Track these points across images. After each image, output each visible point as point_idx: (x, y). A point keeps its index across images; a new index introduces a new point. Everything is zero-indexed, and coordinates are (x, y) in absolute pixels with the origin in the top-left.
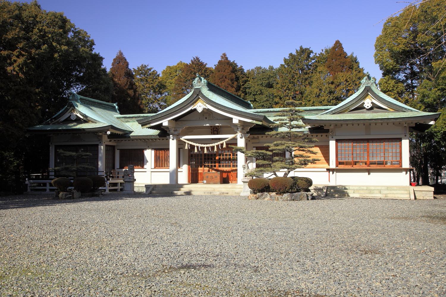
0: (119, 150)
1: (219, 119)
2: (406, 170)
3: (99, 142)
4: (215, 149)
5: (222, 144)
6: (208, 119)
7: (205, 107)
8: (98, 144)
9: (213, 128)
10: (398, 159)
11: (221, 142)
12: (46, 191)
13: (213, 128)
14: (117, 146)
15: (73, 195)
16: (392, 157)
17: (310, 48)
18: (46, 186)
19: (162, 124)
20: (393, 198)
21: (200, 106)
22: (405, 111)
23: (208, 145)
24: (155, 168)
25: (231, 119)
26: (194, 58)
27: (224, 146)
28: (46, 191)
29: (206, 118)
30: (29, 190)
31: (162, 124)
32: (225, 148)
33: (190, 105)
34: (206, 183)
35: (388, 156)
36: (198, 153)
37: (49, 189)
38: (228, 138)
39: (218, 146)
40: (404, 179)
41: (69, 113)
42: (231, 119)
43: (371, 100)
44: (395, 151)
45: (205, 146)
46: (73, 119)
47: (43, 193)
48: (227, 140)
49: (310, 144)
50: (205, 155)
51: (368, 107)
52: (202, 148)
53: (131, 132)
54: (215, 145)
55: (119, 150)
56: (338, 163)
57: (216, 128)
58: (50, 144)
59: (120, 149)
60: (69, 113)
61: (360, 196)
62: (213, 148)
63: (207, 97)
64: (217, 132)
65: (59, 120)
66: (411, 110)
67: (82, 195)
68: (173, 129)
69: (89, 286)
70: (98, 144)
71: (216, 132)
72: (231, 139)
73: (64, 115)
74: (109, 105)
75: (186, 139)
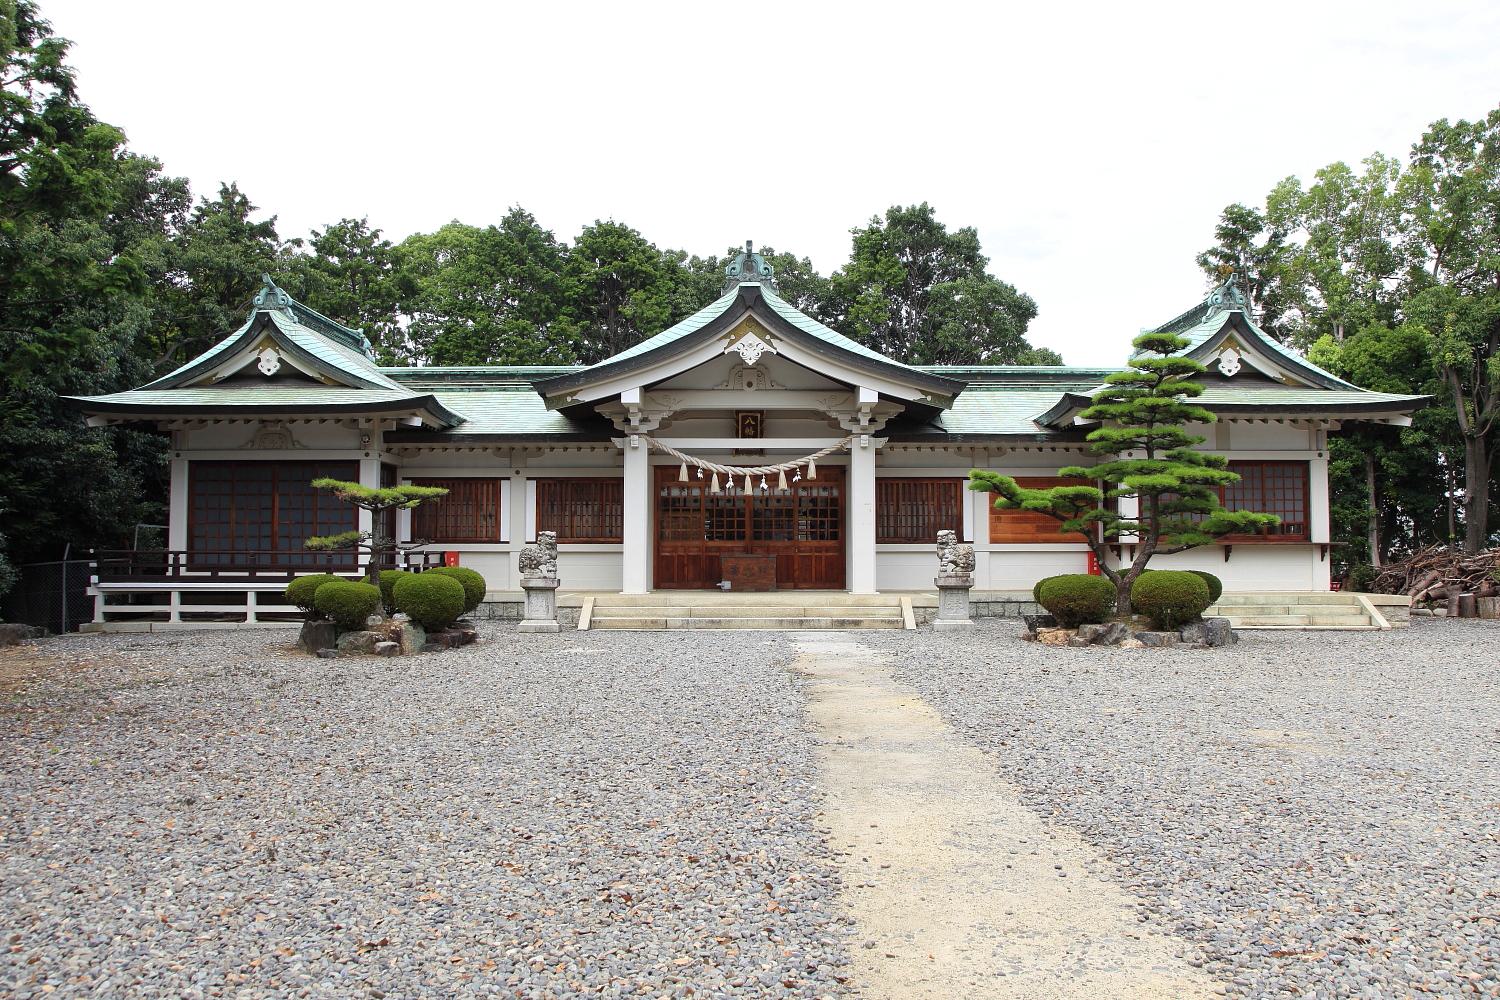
1: (793, 390)
2: (1323, 548)
3: (364, 452)
4: (783, 484)
5: (804, 468)
7: (768, 348)
8: (358, 461)
9: (743, 417)
10: (1300, 518)
11: (801, 461)
13: (744, 418)
14: (402, 467)
19: (618, 396)
20: (1337, 627)
21: (751, 348)
23: (756, 471)
24: (412, 542)
25: (852, 389)
27: (812, 473)
29: (750, 385)
30: (98, 618)
31: (618, 396)
32: (812, 481)
33: (720, 339)
34: (729, 591)
35: (1294, 511)
36: (722, 494)
38: (821, 449)
39: (790, 474)
40: (1319, 572)
42: (852, 389)
43: (1239, 354)
45: (747, 471)
46: (269, 374)
47: (158, 625)
48: (820, 454)
50: (715, 499)
51: (1230, 371)
52: (739, 480)
53: (462, 421)
54: (782, 467)
57: (751, 417)
61: (1242, 624)
62: (773, 479)
63: (293, 339)
64: (755, 429)
65: (216, 374)
67: (427, 641)
68: (640, 416)
70: (358, 461)
72: (832, 453)
74: (348, 335)
75: (681, 450)
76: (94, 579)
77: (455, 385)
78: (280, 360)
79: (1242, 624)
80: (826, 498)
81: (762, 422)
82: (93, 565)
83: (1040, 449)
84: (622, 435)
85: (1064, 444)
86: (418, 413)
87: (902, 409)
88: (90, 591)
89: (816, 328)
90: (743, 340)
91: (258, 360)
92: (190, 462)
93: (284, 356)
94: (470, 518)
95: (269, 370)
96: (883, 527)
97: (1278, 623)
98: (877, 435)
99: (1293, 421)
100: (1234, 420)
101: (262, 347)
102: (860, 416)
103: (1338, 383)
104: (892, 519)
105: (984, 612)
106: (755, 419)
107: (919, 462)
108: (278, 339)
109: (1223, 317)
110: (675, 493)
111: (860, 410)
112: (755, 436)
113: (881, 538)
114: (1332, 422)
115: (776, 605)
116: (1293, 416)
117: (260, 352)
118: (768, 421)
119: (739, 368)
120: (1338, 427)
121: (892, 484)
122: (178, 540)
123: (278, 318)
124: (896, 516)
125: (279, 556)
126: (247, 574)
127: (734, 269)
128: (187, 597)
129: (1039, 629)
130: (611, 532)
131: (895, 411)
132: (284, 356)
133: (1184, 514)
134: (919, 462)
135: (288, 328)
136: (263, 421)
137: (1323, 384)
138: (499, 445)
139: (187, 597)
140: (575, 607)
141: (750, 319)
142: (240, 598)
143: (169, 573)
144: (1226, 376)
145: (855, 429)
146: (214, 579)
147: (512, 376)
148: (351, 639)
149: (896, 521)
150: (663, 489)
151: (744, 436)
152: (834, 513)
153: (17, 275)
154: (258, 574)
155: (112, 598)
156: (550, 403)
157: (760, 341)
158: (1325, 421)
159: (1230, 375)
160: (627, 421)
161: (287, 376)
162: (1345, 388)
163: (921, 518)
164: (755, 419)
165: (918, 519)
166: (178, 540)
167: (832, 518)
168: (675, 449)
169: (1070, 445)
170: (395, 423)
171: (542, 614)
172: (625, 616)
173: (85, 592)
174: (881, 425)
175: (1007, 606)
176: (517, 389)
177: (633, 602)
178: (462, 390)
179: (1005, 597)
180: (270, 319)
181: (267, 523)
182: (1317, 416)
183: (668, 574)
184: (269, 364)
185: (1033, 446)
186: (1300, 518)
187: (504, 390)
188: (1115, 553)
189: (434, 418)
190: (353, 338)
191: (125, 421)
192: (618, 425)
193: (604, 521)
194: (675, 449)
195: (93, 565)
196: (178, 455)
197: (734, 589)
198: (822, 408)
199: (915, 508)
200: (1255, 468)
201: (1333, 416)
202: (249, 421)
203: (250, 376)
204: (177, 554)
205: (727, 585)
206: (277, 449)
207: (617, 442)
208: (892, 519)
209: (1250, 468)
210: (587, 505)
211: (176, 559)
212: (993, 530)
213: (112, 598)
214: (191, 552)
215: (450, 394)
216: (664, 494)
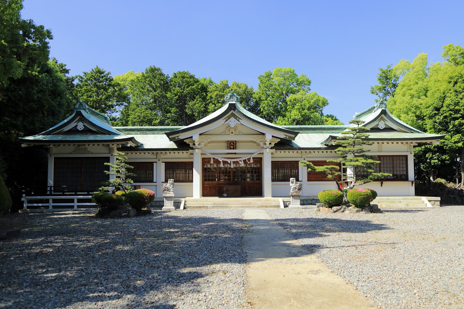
0: (164, 163)
5: (249, 159)
6: (234, 134)
9: (230, 143)
12: (49, 209)
13: (230, 143)
15: (129, 213)
16: (384, 167)
17: (83, 72)
18: (48, 202)
22: (413, 132)
26: (108, 74)
28: (49, 208)
29: (232, 133)
37: (52, 206)
41: (75, 122)
44: (404, 165)
49: (330, 159)
55: (164, 163)
56: (204, 169)
58: (48, 156)
59: (165, 162)
60: (75, 122)
64: (234, 146)
65: (63, 130)
66: (422, 133)
69: (35, 301)
71: (232, 147)
73: (69, 125)
76: (24, 195)
77: (138, 132)
78: (84, 126)
79: (386, 206)
80: (256, 168)
81: (236, 144)
82: (24, 191)
83: (323, 152)
84: (192, 149)
85: (330, 151)
86: (129, 142)
87: (279, 140)
88: (23, 199)
89: (252, 116)
90: (230, 120)
91: (77, 126)
92: (55, 158)
93: (85, 124)
94: (184, 174)
95: (80, 129)
96: (274, 177)
97: (397, 206)
98: (272, 148)
99: (402, 143)
100: (383, 143)
101: (78, 121)
102: (266, 143)
103: (416, 131)
104: (277, 174)
105: (306, 203)
106: (234, 143)
107: (285, 155)
108: (83, 119)
109: (379, 111)
110: (209, 166)
111: (266, 141)
112: (234, 149)
113: (273, 180)
114: (414, 143)
115: (242, 201)
116: (402, 142)
117: (77, 123)
118: (237, 144)
119: (229, 128)
120: (417, 145)
121: (277, 163)
122: (51, 182)
123: (83, 112)
124: (278, 173)
125: (164, 181)
126: (87, 193)
127: (227, 98)
128: (55, 201)
129: (320, 208)
130: (188, 178)
131: (277, 141)
132: (85, 124)
133: (405, 172)
134: (285, 155)
135: (87, 115)
136: (79, 145)
137: (412, 131)
138: (153, 152)
139: (55, 201)
140: (179, 202)
141: (232, 114)
142: (72, 201)
143: (48, 193)
144: (380, 129)
145: (265, 147)
146: (64, 195)
147: (156, 130)
148: (114, 213)
149: (278, 175)
150: (205, 165)
151: (230, 149)
152: (258, 172)
153: (36, 107)
154: (78, 193)
155: (29, 202)
156: (171, 139)
157: (236, 120)
158: (412, 143)
159: (382, 129)
160: (194, 144)
161: (86, 131)
162: (418, 132)
163: (282, 172)
164: (234, 143)
165: (286, 172)
166: (51, 182)
167: (258, 172)
168: (209, 153)
169: (332, 151)
170: (121, 145)
171: (169, 205)
172: (194, 205)
173: (21, 199)
174: (273, 145)
175: (313, 201)
176: (158, 134)
177: (196, 200)
178: (140, 134)
179: (312, 198)
180: (81, 113)
181: (400, 170)
182: (409, 142)
183: (206, 192)
184: (81, 127)
185: (320, 151)
186: (405, 173)
187: (154, 134)
188: (346, 184)
189: (133, 144)
190: (104, 117)
191: (34, 145)
192: (191, 145)
193: (186, 175)
194: (209, 153)
195: (24, 191)
196: (159, 160)
197: (227, 197)
198: (254, 140)
199: (286, 170)
200: (384, 158)
201: (414, 142)
202: (75, 145)
203: (74, 131)
204: (51, 187)
205: (225, 195)
206: (83, 153)
207: (191, 151)
208: (277, 174)
209: (386, 157)
210: (181, 170)
211: (51, 189)
212: (308, 177)
213: (29, 202)
214: (55, 186)
215: (137, 135)
216: (205, 167)
